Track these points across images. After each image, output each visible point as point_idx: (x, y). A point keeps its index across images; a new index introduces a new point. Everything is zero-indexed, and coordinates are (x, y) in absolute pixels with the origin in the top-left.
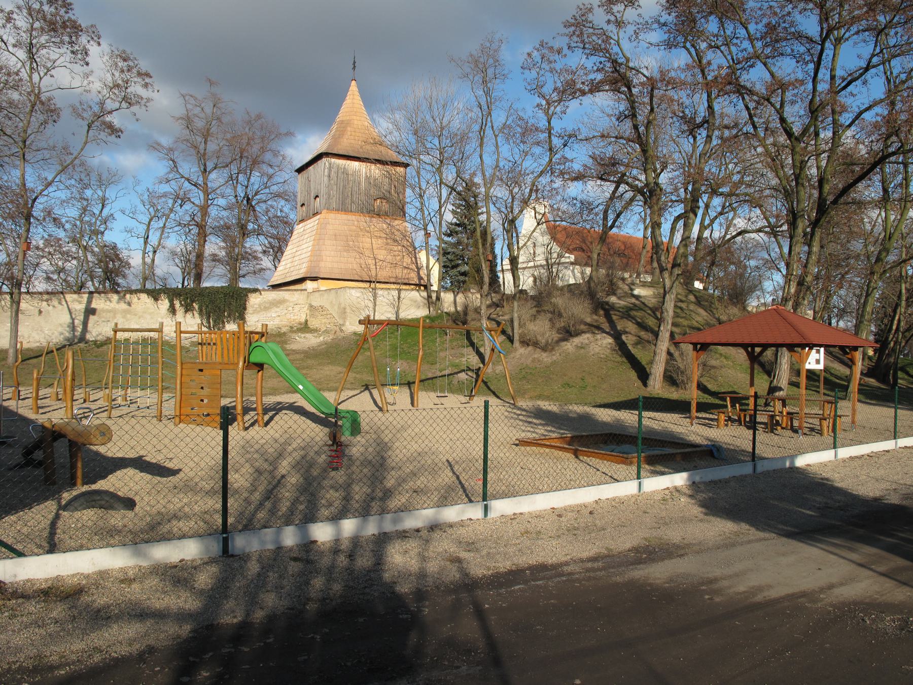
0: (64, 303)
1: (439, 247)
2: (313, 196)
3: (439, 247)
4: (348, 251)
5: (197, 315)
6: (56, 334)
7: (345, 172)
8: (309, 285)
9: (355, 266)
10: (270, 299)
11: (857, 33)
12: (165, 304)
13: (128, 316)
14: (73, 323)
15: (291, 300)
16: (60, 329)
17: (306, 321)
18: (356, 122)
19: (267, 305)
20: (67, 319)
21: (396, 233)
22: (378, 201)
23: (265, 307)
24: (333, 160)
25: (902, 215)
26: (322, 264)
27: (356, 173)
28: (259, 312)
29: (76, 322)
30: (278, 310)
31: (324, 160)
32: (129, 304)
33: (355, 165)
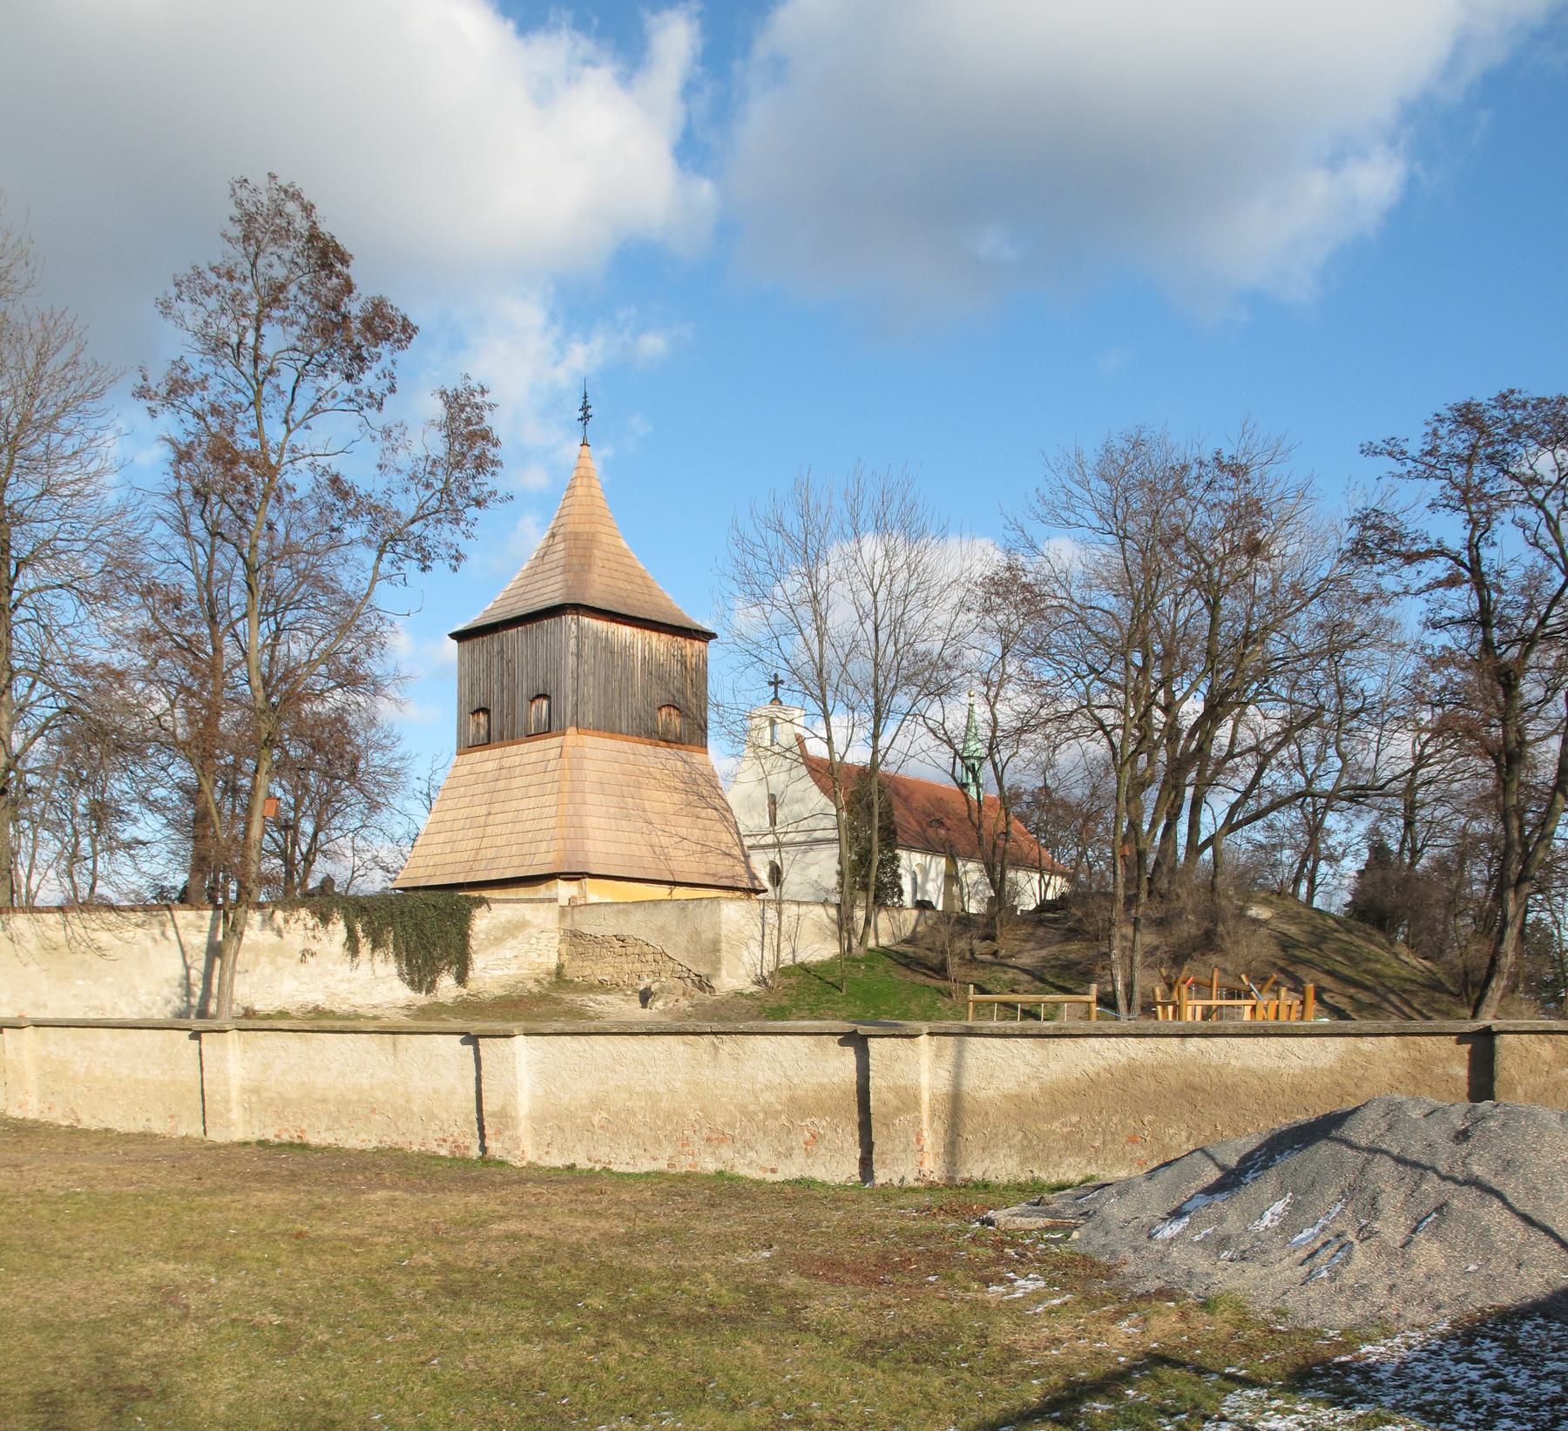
0: (170, 932)
1: (169, 824)
2: (524, 690)
3: (169, 824)
4: (628, 818)
5: (392, 958)
6: (160, 1002)
7: (607, 646)
8: (564, 890)
9: (645, 851)
10: (503, 919)
11: (1351, 997)
12: (339, 930)
13: (280, 959)
14: (187, 977)
15: (536, 921)
16: (166, 992)
17: (560, 967)
18: (604, 538)
19: (499, 934)
20: (175, 968)
21: (701, 780)
22: (664, 711)
23: (496, 938)
24: (586, 621)
25: (1211, 1372)
26: (589, 845)
27: (627, 648)
28: (487, 948)
29: (193, 973)
30: (514, 943)
31: (569, 619)
32: (280, 933)
33: (626, 632)
